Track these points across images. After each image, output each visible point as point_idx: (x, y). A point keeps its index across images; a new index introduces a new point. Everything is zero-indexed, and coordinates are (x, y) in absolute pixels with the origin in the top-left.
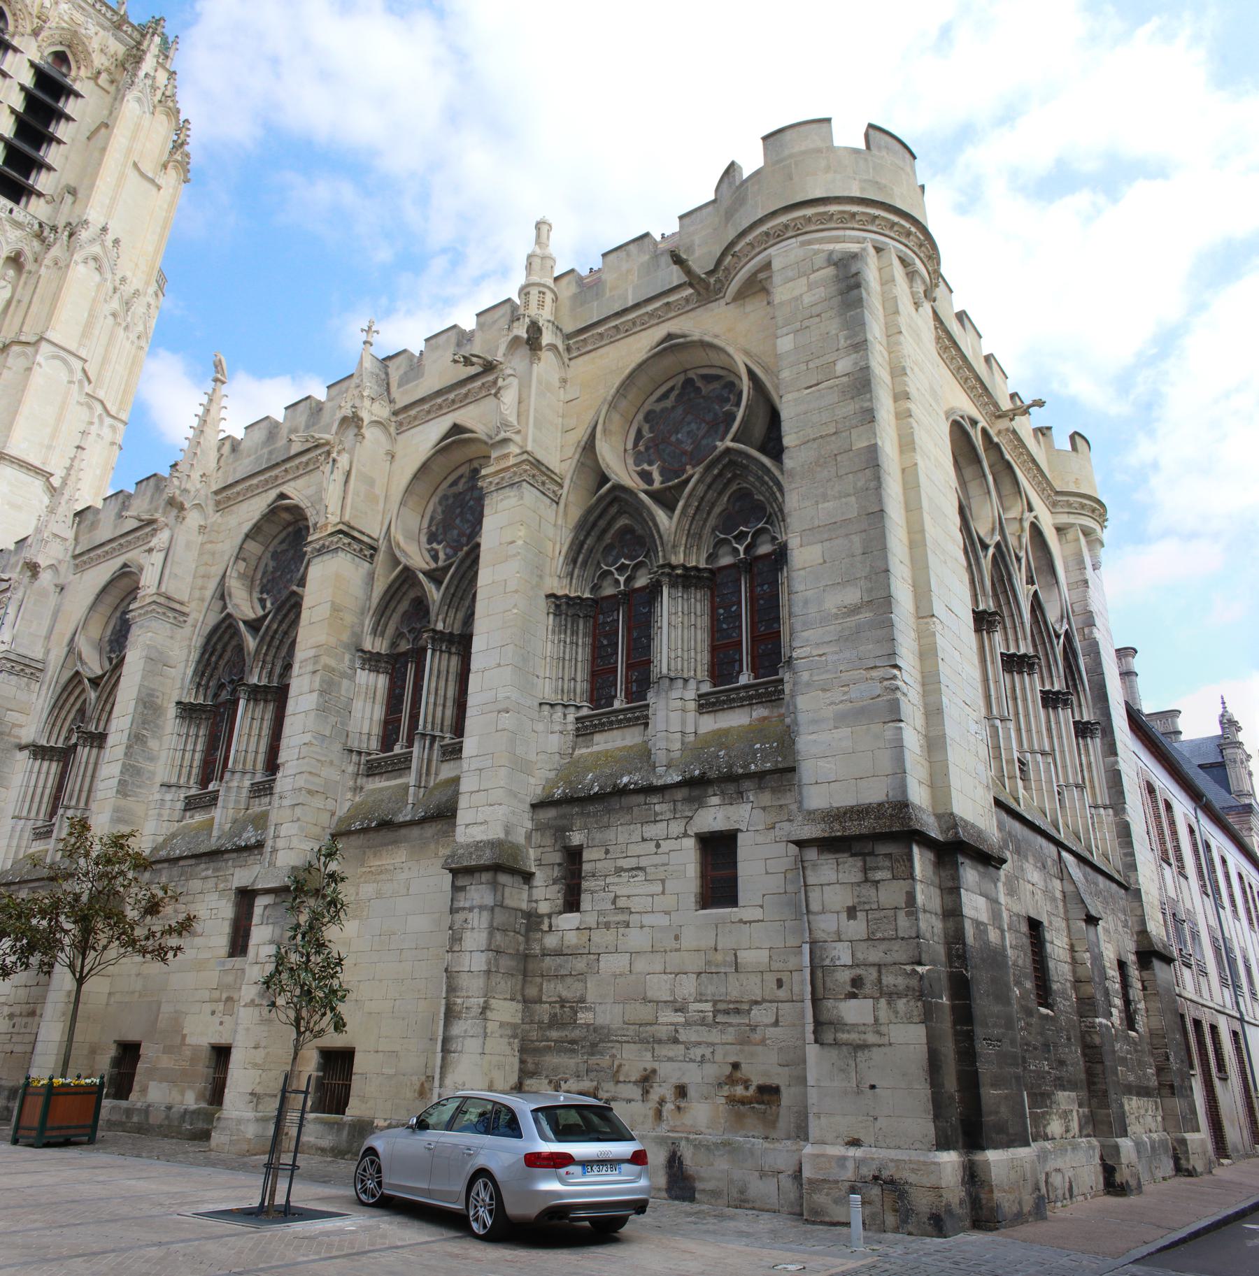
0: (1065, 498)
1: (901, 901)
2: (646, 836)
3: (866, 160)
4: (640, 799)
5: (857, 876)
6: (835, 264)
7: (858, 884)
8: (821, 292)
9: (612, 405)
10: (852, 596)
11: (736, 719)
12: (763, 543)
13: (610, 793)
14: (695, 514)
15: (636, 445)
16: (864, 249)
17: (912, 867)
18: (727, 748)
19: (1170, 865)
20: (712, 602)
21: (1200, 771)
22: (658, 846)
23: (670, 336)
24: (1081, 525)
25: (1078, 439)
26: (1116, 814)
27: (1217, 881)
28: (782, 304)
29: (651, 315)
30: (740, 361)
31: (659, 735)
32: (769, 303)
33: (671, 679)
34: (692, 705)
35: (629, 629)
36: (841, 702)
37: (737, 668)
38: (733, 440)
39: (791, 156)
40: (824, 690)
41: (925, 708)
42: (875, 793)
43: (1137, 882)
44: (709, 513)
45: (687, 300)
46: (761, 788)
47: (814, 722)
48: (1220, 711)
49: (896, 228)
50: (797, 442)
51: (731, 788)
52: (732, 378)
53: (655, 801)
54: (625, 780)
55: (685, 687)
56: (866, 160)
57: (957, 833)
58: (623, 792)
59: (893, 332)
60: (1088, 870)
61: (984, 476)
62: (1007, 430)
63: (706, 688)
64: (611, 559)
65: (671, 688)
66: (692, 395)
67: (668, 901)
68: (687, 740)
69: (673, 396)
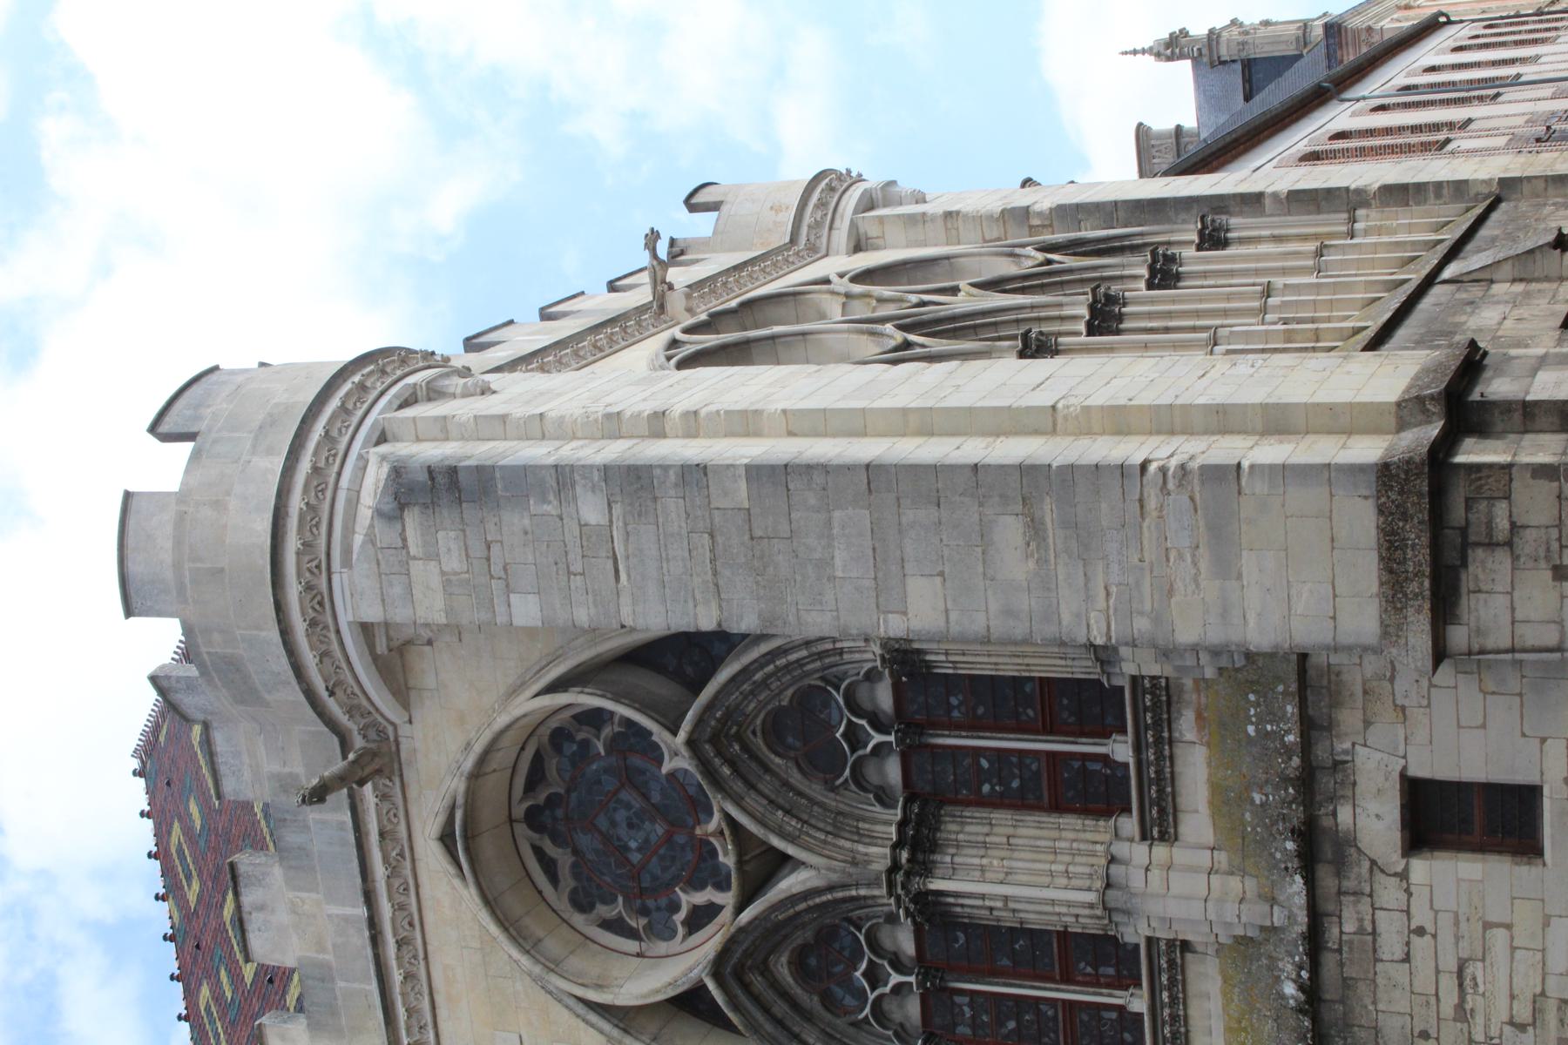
0: (804, 230)
1: (1547, 488)
2: (1399, 955)
3: (215, 442)
4: (1329, 961)
5: (1502, 559)
6: (402, 507)
7: (1515, 558)
8: (447, 539)
9: (553, 965)
10: (1010, 531)
11: (1195, 771)
12: (873, 699)
13: (1314, 1021)
14: (799, 819)
15: (632, 934)
16: (383, 458)
17: (1491, 466)
18: (1248, 788)
19: (1448, 141)
20: (968, 803)
21: (1257, 99)
22: (1420, 931)
23: (446, 839)
24: (856, 212)
25: (700, 198)
26: (1366, 204)
27: (1471, 82)
28: (449, 611)
29: (393, 872)
30: (528, 705)
31: (1212, 916)
32: (430, 643)
33: (1108, 886)
34: (1160, 851)
35: (994, 974)
36: (1195, 564)
37: (1097, 766)
38: (675, 734)
39: (177, 566)
40: (1171, 592)
41: (1213, 433)
42: (1360, 519)
43: (1488, 182)
44: (800, 794)
45: (384, 797)
46: (1329, 727)
47: (1225, 614)
48: (1149, 59)
49: (350, 406)
50: (714, 605)
51: (1325, 782)
52: (545, 731)
53: (1336, 931)
54: (1290, 989)
55: (1126, 863)
56: (215, 442)
57: (1432, 397)
58: (1312, 992)
59: (538, 427)
60: (1470, 247)
61: (773, 338)
62: (688, 296)
63: (1129, 824)
64: (849, 1001)
65: (1125, 888)
66: (560, 813)
67: (1526, 918)
68: (1224, 865)
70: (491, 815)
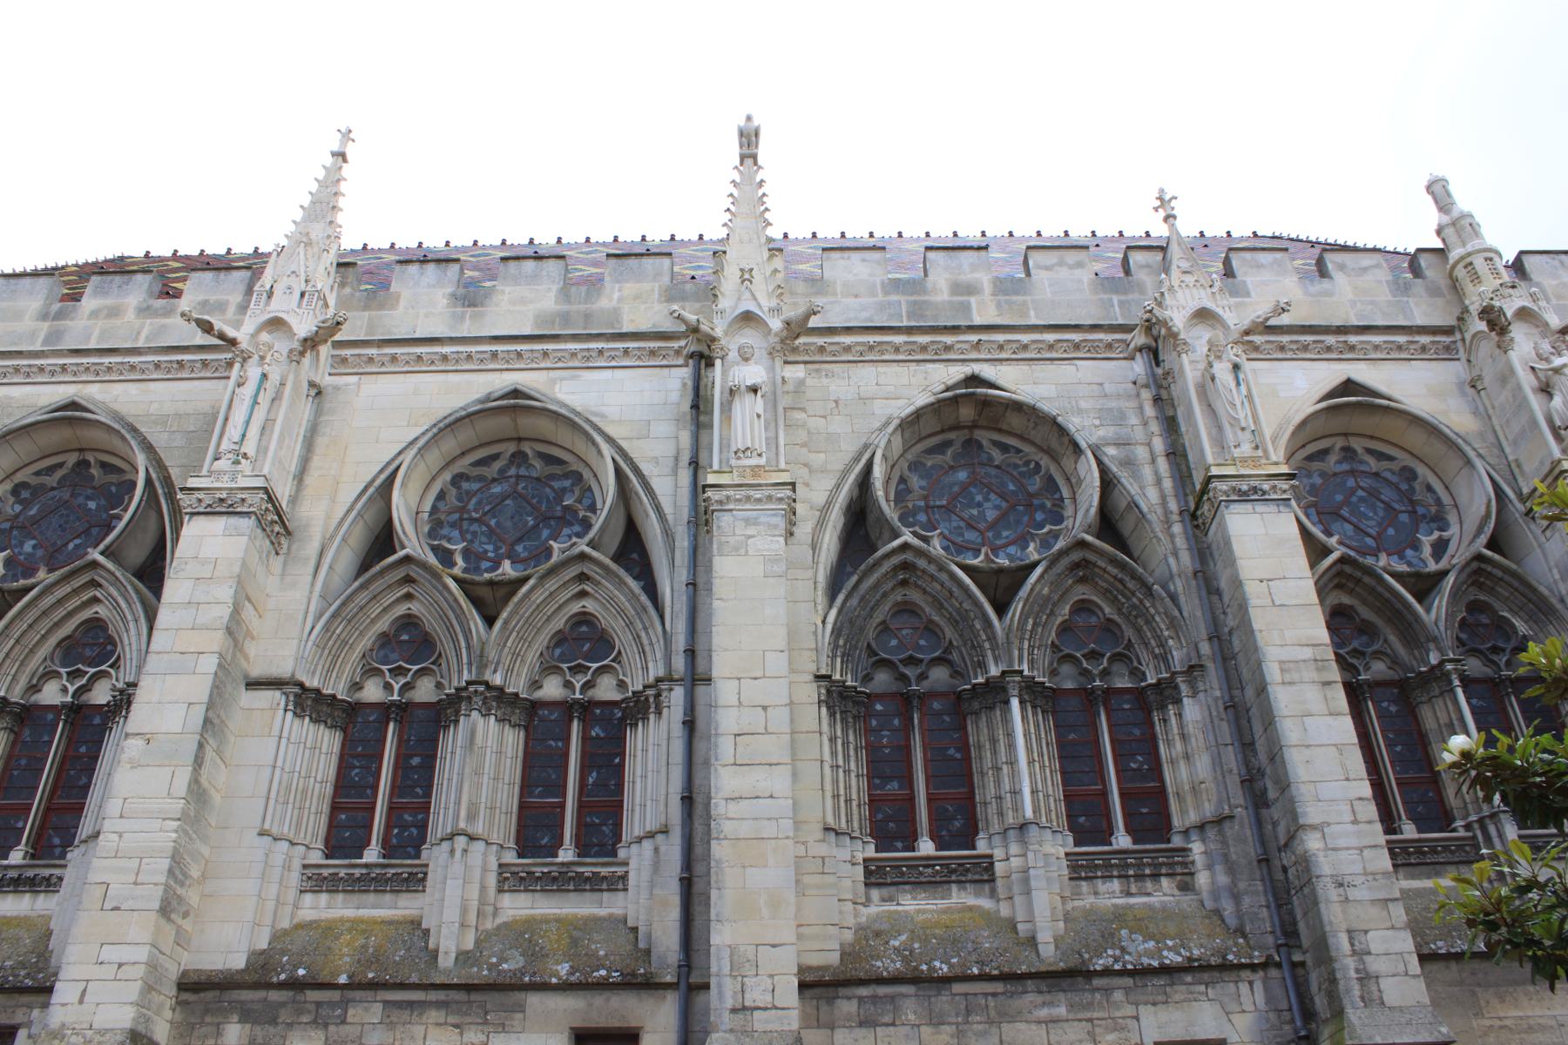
11: (913, 904)
38: (102, 553)
52: (576, 466)
69: (59, 474)
70: (527, 424)
